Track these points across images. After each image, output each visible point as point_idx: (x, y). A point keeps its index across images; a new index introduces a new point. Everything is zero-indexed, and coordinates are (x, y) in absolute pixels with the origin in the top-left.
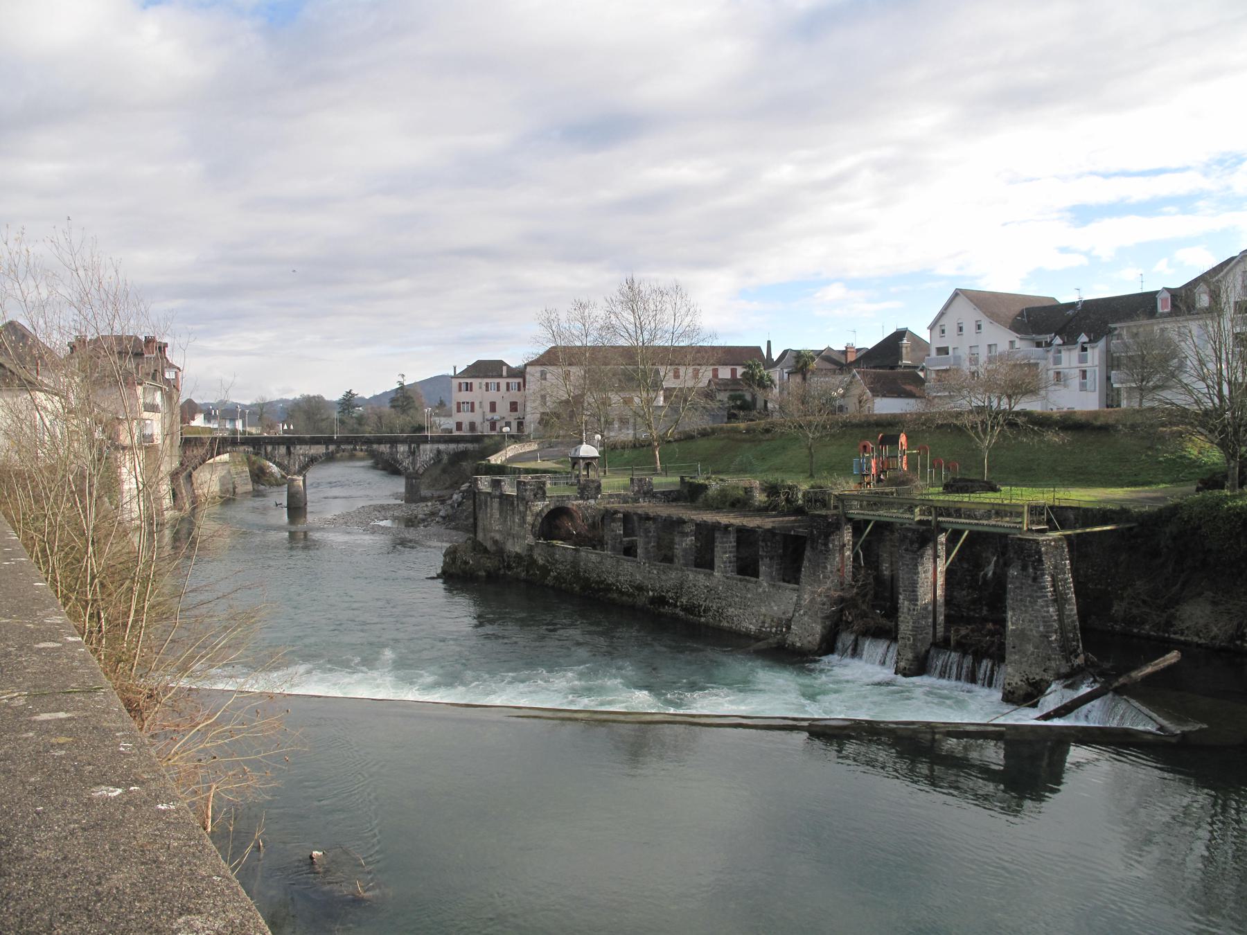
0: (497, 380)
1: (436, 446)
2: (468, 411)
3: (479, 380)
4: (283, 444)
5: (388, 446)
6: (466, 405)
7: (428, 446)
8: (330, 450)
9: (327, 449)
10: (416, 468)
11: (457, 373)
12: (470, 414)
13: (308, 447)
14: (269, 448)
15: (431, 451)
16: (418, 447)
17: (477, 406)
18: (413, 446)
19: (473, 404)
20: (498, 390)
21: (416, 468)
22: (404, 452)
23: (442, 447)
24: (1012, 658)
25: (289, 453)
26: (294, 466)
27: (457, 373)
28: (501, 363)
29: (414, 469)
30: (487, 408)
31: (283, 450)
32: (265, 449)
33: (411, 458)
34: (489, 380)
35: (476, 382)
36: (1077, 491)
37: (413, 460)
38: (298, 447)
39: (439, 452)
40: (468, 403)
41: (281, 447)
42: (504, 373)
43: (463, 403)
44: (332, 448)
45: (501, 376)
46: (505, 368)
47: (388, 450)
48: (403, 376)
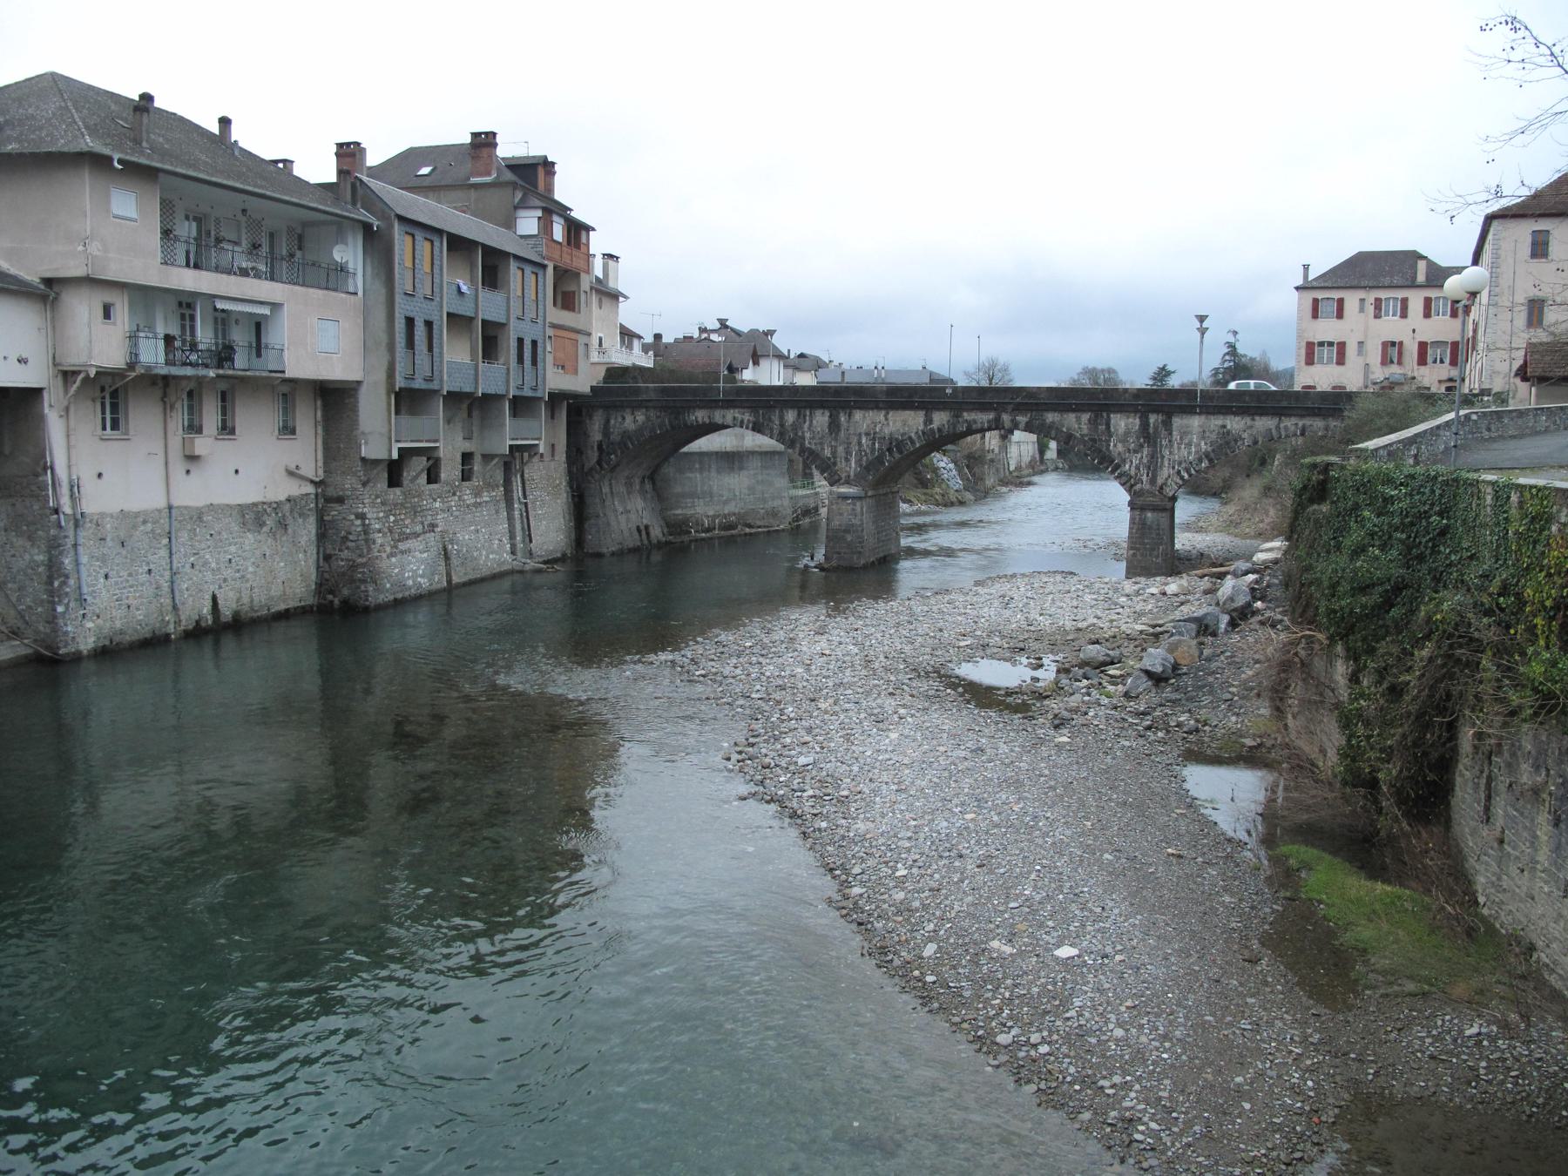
0: (1400, 294)
1: (1216, 422)
2: (1330, 361)
3: (1361, 294)
4: (823, 407)
5: (1085, 417)
6: (1326, 349)
7: (1195, 422)
8: (935, 426)
9: (929, 421)
10: (1160, 481)
11: (1311, 278)
12: (1334, 322)
13: (881, 416)
14: (790, 416)
15: (1203, 435)
16: (1167, 424)
17: (1351, 351)
18: (1152, 418)
19: (1342, 346)
20: (1404, 315)
21: (1160, 481)
22: (1127, 433)
23: (1235, 424)
24: (1555, 511)
25: (834, 426)
26: (847, 460)
27: (1311, 278)
28: (1415, 256)
29: (1153, 481)
30: (1375, 357)
31: (821, 419)
32: (782, 418)
33: (1145, 451)
34: (1383, 294)
35: (1352, 299)
36: (1182, 419)
37: (1153, 456)
38: (858, 415)
39: (1225, 433)
40: (1331, 344)
41: (818, 413)
42: (1421, 278)
43: (1321, 344)
44: (940, 419)
45: (1413, 285)
46: (1422, 265)
47: (1085, 429)
48: (1235, 333)
